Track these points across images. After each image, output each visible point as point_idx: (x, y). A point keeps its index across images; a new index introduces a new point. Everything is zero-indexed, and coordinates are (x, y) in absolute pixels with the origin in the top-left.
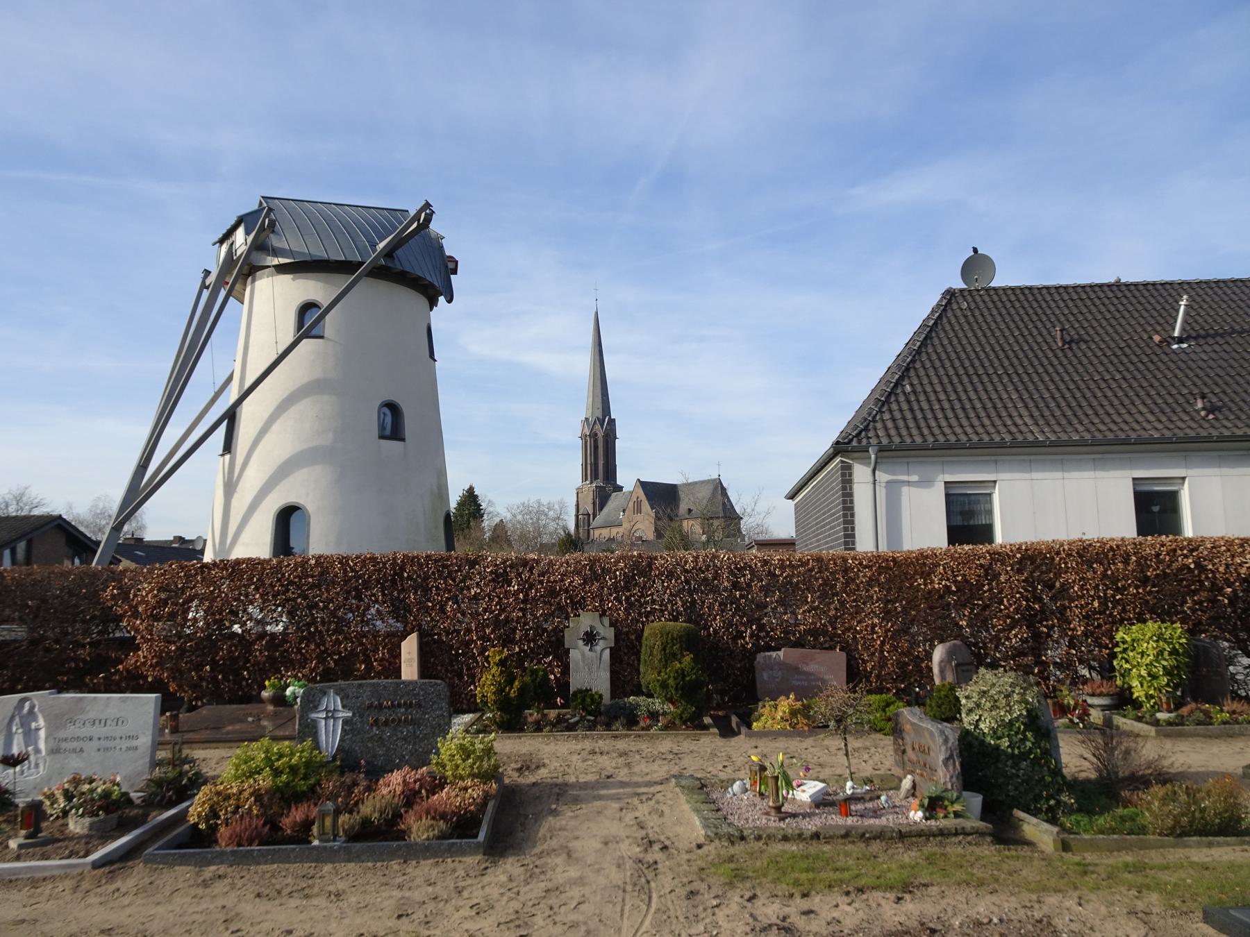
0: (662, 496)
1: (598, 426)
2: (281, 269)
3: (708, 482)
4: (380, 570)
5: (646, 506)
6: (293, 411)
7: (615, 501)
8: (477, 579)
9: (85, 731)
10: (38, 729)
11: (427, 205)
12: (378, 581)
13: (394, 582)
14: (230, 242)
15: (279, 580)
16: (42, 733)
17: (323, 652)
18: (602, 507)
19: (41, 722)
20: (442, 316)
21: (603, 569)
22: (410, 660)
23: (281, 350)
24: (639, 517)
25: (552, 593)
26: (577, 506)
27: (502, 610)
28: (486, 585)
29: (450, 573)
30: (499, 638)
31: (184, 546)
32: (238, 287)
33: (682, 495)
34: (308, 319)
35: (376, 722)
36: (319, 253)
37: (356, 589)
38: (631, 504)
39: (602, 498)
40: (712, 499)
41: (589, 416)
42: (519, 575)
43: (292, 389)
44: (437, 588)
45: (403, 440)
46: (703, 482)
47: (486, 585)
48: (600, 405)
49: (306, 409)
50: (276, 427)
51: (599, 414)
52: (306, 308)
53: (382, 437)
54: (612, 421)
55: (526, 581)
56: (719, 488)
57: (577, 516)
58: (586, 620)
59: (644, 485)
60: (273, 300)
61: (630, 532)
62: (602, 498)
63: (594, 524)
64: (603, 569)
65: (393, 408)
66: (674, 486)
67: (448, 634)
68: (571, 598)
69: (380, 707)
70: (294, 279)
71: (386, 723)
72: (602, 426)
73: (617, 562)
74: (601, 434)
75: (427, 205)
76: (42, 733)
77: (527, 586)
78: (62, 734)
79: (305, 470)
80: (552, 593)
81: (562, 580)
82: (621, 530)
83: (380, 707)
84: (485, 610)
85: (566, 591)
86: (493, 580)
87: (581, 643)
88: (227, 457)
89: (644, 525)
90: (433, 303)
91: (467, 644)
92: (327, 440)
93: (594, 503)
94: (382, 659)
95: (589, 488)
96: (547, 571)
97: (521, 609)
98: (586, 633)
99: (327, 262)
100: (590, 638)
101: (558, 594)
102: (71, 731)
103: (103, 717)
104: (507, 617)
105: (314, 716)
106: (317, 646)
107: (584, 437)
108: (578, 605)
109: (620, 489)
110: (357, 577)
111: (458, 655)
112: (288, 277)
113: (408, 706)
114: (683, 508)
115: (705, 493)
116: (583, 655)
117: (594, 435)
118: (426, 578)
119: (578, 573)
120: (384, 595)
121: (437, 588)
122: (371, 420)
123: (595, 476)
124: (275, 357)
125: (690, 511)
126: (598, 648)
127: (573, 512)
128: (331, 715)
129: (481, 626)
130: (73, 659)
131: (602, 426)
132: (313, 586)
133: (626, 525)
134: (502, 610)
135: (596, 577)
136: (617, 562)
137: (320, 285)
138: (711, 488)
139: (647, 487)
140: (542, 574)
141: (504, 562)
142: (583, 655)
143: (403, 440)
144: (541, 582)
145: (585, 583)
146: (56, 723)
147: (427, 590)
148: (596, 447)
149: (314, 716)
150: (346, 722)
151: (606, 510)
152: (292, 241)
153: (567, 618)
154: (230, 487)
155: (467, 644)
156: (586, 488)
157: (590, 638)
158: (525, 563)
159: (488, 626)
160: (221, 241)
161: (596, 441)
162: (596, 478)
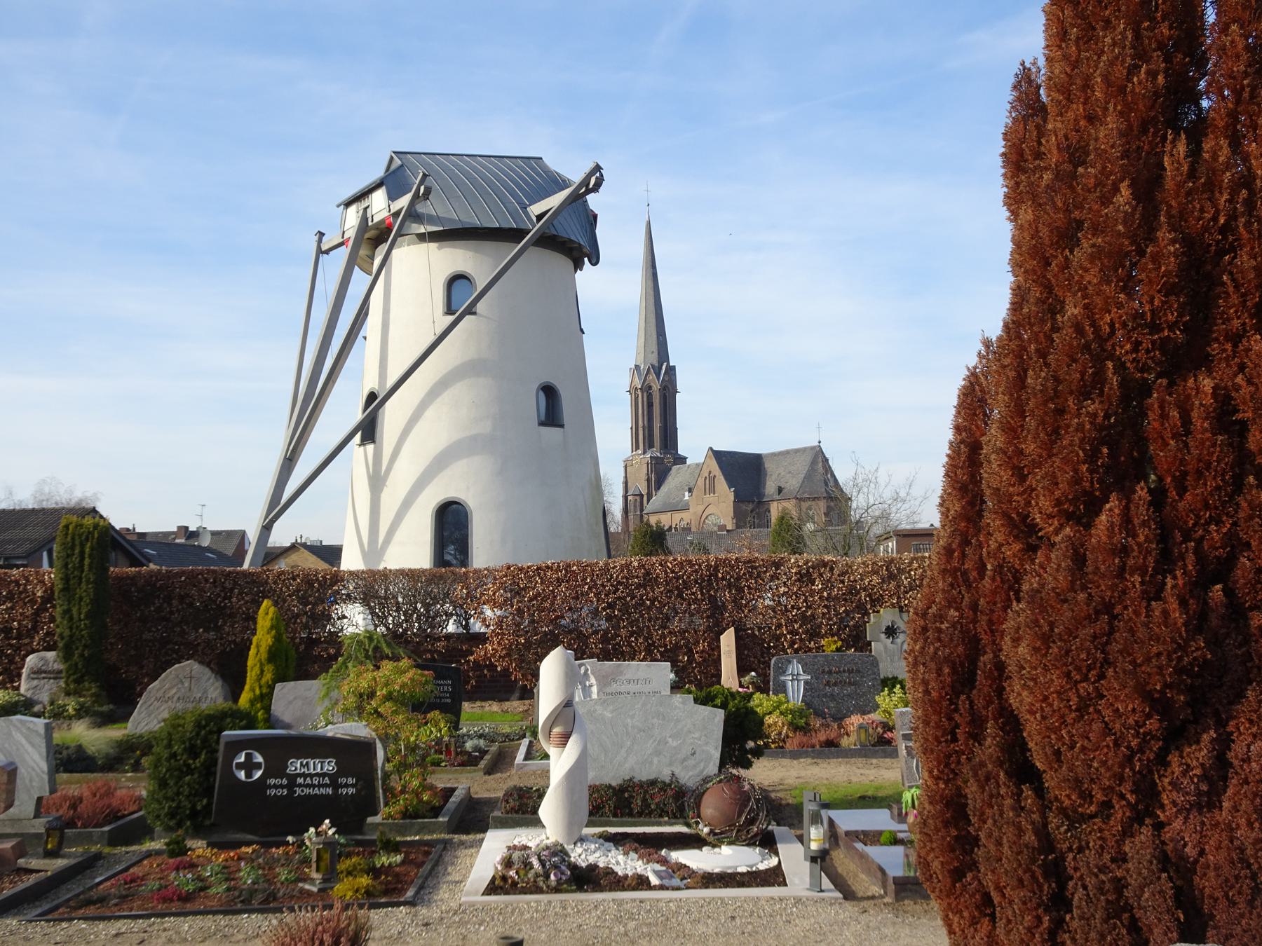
0: (743, 472)
1: (652, 376)
2: (422, 237)
3: (804, 450)
4: (696, 571)
5: (721, 484)
6: (446, 397)
7: (676, 477)
8: (784, 578)
9: (623, 688)
10: (591, 686)
11: (598, 168)
12: (696, 582)
13: (710, 584)
14: (364, 204)
15: (609, 581)
16: (595, 689)
17: (650, 645)
18: (659, 485)
19: (593, 680)
20: (586, 277)
21: (898, 569)
22: (729, 652)
23: (439, 331)
24: (710, 498)
25: (852, 591)
26: (626, 483)
27: (808, 607)
28: (793, 585)
29: (759, 573)
30: (806, 632)
31: (190, 542)
32: (363, 252)
33: (769, 465)
34: (458, 295)
35: (828, 683)
36: (473, 219)
37: (677, 588)
38: (701, 482)
39: (659, 473)
40: (809, 477)
41: (641, 362)
42: (821, 575)
43: (445, 372)
44: (749, 587)
45: (562, 426)
46: (797, 451)
47: (793, 585)
48: (654, 348)
49: (462, 392)
50: (429, 413)
51: (654, 359)
52: (456, 280)
53: (542, 424)
54: (671, 370)
55: (828, 581)
56: (818, 458)
57: (625, 497)
58: (887, 616)
59: (719, 456)
60: (418, 270)
61: (702, 520)
62: (659, 473)
63: (648, 508)
64: (898, 569)
65: (549, 392)
66: (758, 458)
67: (760, 629)
68: (870, 595)
69: (830, 672)
70: (439, 248)
71: (835, 684)
72: (658, 375)
73: (911, 563)
74: (656, 387)
75: (598, 168)
76: (595, 689)
77: (828, 584)
78: (608, 690)
79: (465, 461)
80: (852, 591)
81: (862, 580)
82: (686, 517)
83: (830, 672)
84: (793, 607)
85: (865, 589)
86: (798, 580)
87: (883, 636)
88: (370, 448)
89: (719, 508)
90: (578, 265)
91: (777, 638)
92: (485, 427)
93: (649, 480)
94: (703, 651)
95: (643, 460)
96: (847, 572)
97: (825, 606)
98: (888, 628)
99: (476, 229)
100: (891, 632)
101: (858, 593)
102: (614, 687)
103: (636, 677)
104: (812, 615)
105: (783, 678)
106: (646, 639)
107: (633, 391)
108: (877, 601)
109: (683, 460)
110: (678, 578)
111: (769, 647)
112: (433, 246)
113: (850, 672)
114: (770, 488)
115: (802, 466)
116: (885, 647)
117: (647, 389)
118: (739, 578)
119: (876, 573)
120: (702, 594)
121: (749, 587)
122: (532, 405)
123: (650, 444)
124: (432, 339)
125: (780, 490)
126: (899, 641)
127: (619, 491)
128: (795, 678)
129: (790, 622)
130: (429, 651)
131: (658, 375)
132: (639, 586)
133: (695, 509)
134: (808, 607)
135: (891, 577)
136: (911, 563)
137: (469, 254)
138: (808, 458)
139: (722, 458)
140: (843, 574)
141: (806, 563)
142: (885, 647)
143: (562, 426)
144: (843, 582)
145: (883, 581)
146: (603, 681)
147: (740, 590)
148: (650, 405)
149: (783, 678)
150: (806, 683)
151: (664, 489)
152: (440, 208)
153: (867, 614)
154: (377, 481)
155: (777, 638)
156: (638, 459)
157: (891, 632)
158: (825, 564)
159: (796, 622)
160: (348, 204)
161: (650, 397)
162: (651, 446)
